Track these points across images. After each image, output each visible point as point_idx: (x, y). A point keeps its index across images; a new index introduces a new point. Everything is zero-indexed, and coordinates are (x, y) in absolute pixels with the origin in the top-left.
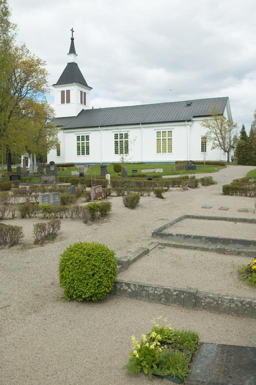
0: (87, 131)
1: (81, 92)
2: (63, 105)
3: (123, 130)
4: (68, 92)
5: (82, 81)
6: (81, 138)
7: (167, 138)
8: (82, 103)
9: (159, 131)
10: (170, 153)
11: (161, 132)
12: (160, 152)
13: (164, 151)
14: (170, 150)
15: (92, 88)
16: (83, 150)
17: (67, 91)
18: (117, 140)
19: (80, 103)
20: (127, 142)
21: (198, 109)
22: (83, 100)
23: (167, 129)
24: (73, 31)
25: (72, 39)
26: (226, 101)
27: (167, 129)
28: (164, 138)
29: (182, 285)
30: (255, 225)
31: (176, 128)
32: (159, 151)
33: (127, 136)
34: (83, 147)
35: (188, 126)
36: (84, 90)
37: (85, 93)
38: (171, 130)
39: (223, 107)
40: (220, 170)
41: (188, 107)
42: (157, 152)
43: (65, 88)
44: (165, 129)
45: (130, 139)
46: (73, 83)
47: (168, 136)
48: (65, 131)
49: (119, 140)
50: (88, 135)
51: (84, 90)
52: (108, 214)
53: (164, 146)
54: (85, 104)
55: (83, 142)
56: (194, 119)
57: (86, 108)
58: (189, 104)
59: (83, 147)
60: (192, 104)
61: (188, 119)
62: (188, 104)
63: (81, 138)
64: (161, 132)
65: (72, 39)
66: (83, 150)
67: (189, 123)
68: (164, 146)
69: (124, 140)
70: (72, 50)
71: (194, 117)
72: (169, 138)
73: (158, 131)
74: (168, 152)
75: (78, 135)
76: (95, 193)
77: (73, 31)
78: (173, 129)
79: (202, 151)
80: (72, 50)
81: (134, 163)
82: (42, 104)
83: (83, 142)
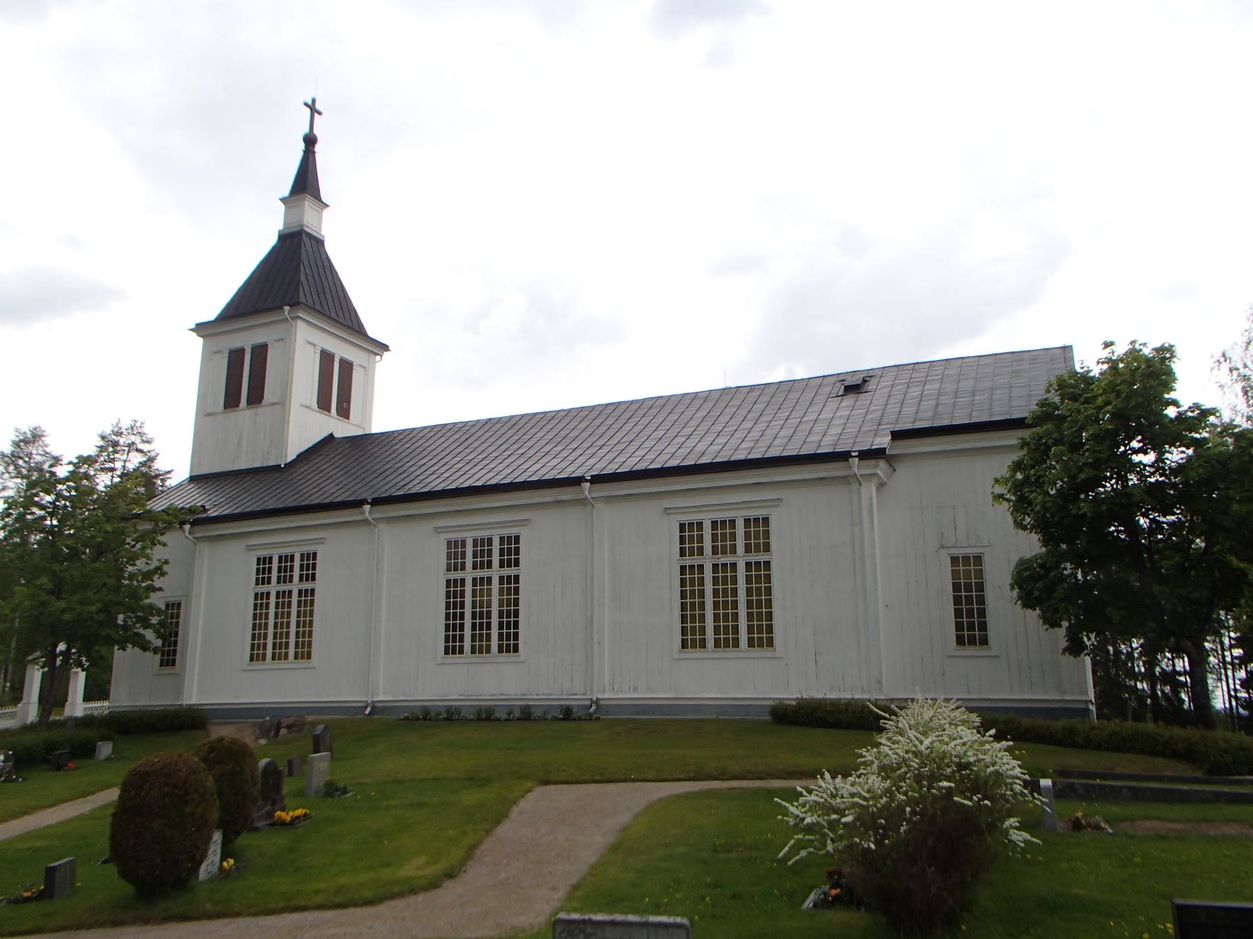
1: (326, 358)
2: (233, 415)
4: (260, 352)
8: (324, 404)
9: (695, 517)
10: (766, 652)
11: (740, 525)
12: (703, 644)
13: (727, 640)
14: (763, 637)
15: (385, 348)
16: (481, 626)
17: (254, 348)
18: (458, 575)
19: (315, 406)
20: (761, 574)
24: (313, 108)
25: (310, 141)
32: (691, 639)
33: (511, 551)
34: (724, 573)
36: (341, 350)
37: (347, 367)
38: (760, 513)
41: (849, 400)
42: (684, 645)
43: (246, 339)
47: (748, 549)
48: (201, 532)
50: (512, 531)
51: (341, 350)
52: (1041, 618)
53: (726, 604)
55: (479, 573)
57: (342, 429)
58: (855, 386)
59: (724, 573)
60: (871, 386)
65: (310, 141)
66: (481, 626)
67: (881, 467)
68: (726, 604)
72: (753, 558)
73: (687, 518)
74: (751, 643)
75: (264, 553)
77: (313, 108)
78: (321, 541)
81: (526, 715)
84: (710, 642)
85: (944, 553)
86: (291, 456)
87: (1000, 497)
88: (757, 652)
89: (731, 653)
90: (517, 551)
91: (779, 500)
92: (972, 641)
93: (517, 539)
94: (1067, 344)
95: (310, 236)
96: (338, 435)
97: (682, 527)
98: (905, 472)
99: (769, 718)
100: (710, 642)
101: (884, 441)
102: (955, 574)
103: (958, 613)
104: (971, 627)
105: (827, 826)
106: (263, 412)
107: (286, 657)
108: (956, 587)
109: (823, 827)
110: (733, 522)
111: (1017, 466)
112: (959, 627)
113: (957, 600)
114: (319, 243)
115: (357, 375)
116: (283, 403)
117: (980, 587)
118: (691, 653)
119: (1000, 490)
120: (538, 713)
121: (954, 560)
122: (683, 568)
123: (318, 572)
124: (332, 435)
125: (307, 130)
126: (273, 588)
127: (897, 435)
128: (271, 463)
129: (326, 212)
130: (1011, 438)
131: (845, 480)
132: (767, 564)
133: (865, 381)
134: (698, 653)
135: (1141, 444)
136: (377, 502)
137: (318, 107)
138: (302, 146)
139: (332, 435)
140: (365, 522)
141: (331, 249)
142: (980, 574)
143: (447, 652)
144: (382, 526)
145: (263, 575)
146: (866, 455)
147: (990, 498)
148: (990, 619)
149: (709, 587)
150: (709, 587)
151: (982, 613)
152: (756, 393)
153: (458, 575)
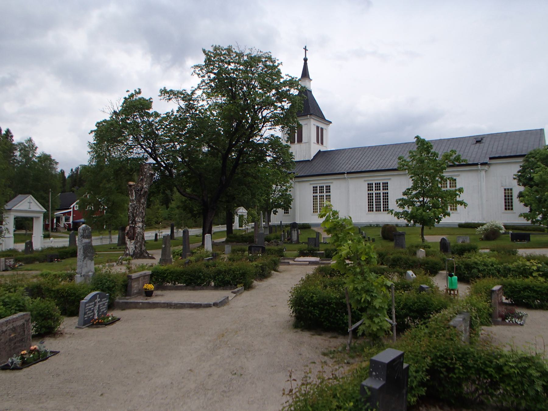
0: (371, 176)
1: (318, 127)
3: (380, 179)
5: (318, 114)
6: (318, 189)
12: (380, 210)
13: (378, 210)
15: (331, 122)
19: (316, 142)
22: (320, 139)
24: (305, 49)
25: (305, 60)
27: (382, 180)
29: (206, 303)
32: (370, 209)
34: (378, 195)
35: (483, 173)
36: (321, 125)
37: (322, 129)
41: (478, 144)
44: (323, 183)
45: (333, 193)
46: (307, 115)
51: (321, 125)
54: (322, 143)
55: (377, 192)
57: (323, 149)
58: (479, 140)
60: (483, 141)
61: (482, 162)
62: (477, 140)
63: (318, 189)
65: (305, 60)
67: (486, 167)
69: (374, 192)
71: (491, 158)
74: (384, 210)
77: (305, 49)
79: (506, 209)
83: (377, 192)
84: (374, 209)
85: (502, 187)
86: (312, 158)
87: (514, 179)
90: (387, 186)
91: (459, 175)
92: (509, 209)
93: (387, 183)
94: (543, 128)
95: (309, 91)
96: (321, 150)
98: (492, 168)
99: (458, 226)
100: (374, 209)
101: (487, 160)
102: (505, 193)
103: (505, 202)
104: (509, 206)
106: (302, 145)
108: (505, 196)
111: (519, 172)
112: (506, 206)
113: (505, 199)
114: (311, 92)
115: (324, 131)
116: (309, 142)
117: (512, 196)
118: (508, 211)
119: (515, 177)
120: (400, 225)
121: (505, 190)
123: (331, 190)
125: (304, 57)
127: (491, 158)
128: (307, 159)
129: (311, 82)
130: (521, 160)
131: (477, 170)
136: (348, 173)
138: (303, 62)
140: (345, 178)
141: (315, 94)
142: (511, 193)
143: (369, 211)
144: (349, 179)
145: (315, 191)
146: (483, 164)
147: (512, 179)
148: (514, 204)
151: (512, 202)
152: (449, 142)
153: (371, 192)
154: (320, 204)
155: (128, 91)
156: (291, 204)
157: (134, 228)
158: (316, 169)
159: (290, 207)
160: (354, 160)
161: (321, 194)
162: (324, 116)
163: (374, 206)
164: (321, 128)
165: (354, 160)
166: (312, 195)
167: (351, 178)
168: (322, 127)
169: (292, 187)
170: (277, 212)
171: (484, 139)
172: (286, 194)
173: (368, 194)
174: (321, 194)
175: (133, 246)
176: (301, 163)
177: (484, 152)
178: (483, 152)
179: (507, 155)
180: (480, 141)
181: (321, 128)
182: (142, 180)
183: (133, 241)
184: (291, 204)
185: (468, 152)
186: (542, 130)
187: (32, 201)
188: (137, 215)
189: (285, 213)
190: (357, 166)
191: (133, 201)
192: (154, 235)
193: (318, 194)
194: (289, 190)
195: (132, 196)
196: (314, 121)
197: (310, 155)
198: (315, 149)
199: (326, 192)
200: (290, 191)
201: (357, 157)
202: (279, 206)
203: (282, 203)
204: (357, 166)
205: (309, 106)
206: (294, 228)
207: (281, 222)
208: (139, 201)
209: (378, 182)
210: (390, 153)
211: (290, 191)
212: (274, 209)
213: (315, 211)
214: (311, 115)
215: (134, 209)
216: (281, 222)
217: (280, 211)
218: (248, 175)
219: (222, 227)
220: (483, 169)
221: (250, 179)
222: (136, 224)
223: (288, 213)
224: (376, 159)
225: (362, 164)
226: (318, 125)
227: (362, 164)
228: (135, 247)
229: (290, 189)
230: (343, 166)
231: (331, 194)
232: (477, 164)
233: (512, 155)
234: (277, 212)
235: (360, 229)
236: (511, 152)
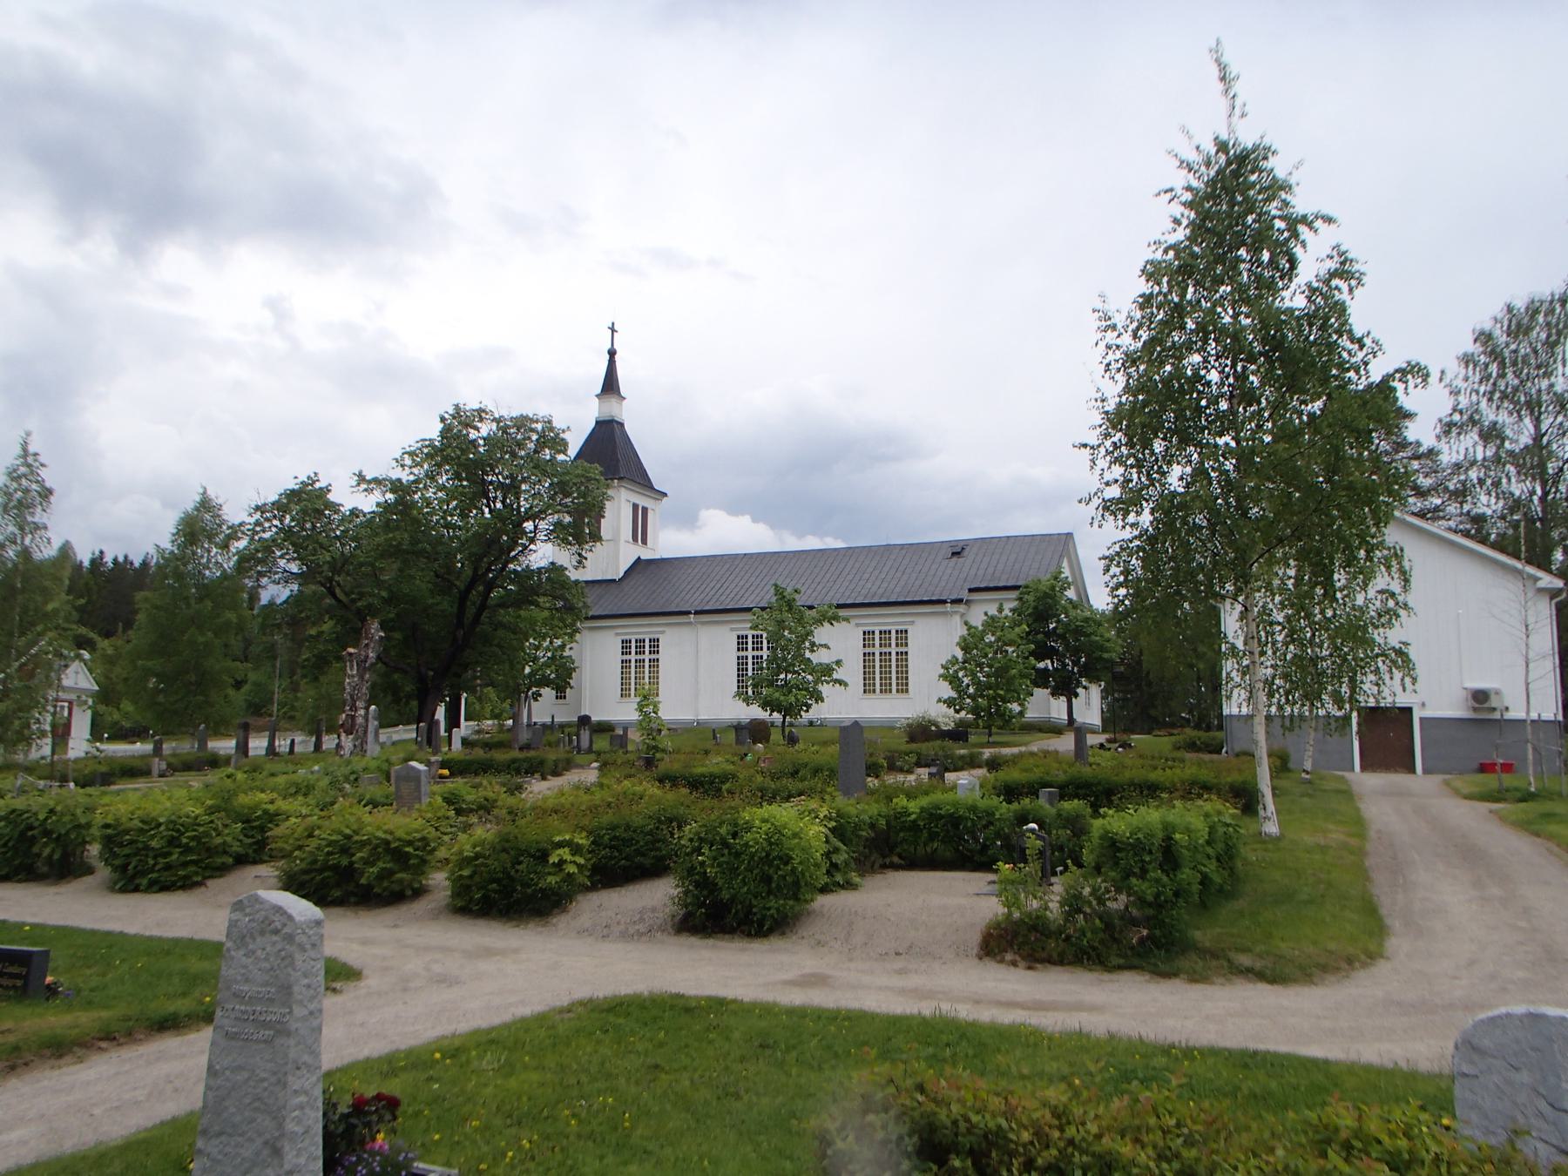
1: (635, 507)
5: (639, 478)
7: (877, 651)
11: (877, 633)
12: (874, 691)
13: (886, 690)
14: (903, 688)
15: (665, 495)
19: (631, 540)
21: (984, 566)
22: (640, 533)
23: (874, 624)
24: (613, 330)
25: (612, 353)
26: (1066, 544)
27: (874, 624)
28: (884, 650)
30: (321, 1175)
31: (668, 630)
34: (885, 656)
36: (642, 502)
37: (645, 510)
39: (1056, 557)
40: (210, 883)
41: (955, 559)
45: (664, 655)
47: (897, 645)
49: (750, 653)
51: (642, 502)
53: (886, 673)
54: (644, 542)
56: (842, 613)
57: (646, 554)
58: (957, 551)
59: (885, 656)
60: (965, 553)
61: (953, 598)
64: (877, 633)
65: (612, 353)
67: (961, 608)
68: (886, 673)
70: (610, 386)
71: (971, 590)
73: (867, 629)
74: (898, 691)
76: (68, 833)
77: (613, 330)
78: (663, 632)
80: (610, 386)
82: (185, 537)
84: (878, 690)
86: (621, 575)
88: (900, 695)
89: (888, 696)
97: (864, 633)
100: (878, 690)
101: (965, 595)
105: (396, 868)
107: (630, 695)
109: (391, 873)
110: (890, 632)
114: (622, 425)
116: (615, 540)
118: (867, 696)
122: (865, 654)
123: (660, 649)
124: (639, 558)
125: (610, 346)
126: (633, 657)
127: (971, 590)
128: (609, 577)
129: (624, 402)
131: (945, 614)
132: (906, 653)
133: (963, 549)
134: (872, 696)
135: (1161, 311)
136: (697, 613)
137: (616, 328)
138: (608, 357)
139: (639, 558)
140: (690, 623)
141: (630, 429)
144: (699, 626)
145: (626, 649)
149: (877, 664)
150: (877, 664)
154: (636, 678)
155: (296, 478)
156: (571, 678)
157: (353, 718)
158: (629, 601)
159: (569, 683)
160: (712, 585)
161: (639, 657)
162: (649, 480)
163: (894, 663)
164: (643, 508)
165: (712, 585)
166: (620, 657)
167: (703, 623)
168: (646, 505)
169: (576, 642)
170: (540, 695)
171: (968, 549)
172: (562, 657)
173: (738, 658)
174: (639, 657)
175: (351, 745)
176: (597, 586)
177: (962, 576)
178: (982, 566)
179: (1001, 584)
180: (958, 553)
181: (643, 508)
182: (367, 645)
183: (351, 737)
184: (571, 678)
185: (1001, 554)
186: (1069, 535)
187: (80, 670)
188: (358, 698)
189: (557, 698)
190: (717, 596)
191: (353, 676)
192: (289, 742)
193: (633, 657)
194: (568, 647)
195: (351, 669)
196: (628, 492)
197: (618, 568)
198: (628, 554)
199: (650, 653)
200: (571, 649)
201: (717, 578)
202: (545, 682)
203: (553, 676)
204: (717, 596)
205: (618, 461)
206: (584, 725)
207: (553, 717)
208: (362, 677)
209: (641, 637)
210: (786, 572)
211: (571, 649)
212: (534, 689)
213: (625, 693)
214: (620, 479)
215: (354, 688)
216: (553, 717)
217: (548, 693)
218: (501, 625)
219: (405, 731)
220: (956, 612)
221: (501, 632)
222: (356, 710)
223: (565, 697)
224: (756, 584)
225: (728, 592)
226: (637, 502)
227: (728, 592)
228: (355, 746)
229: (572, 645)
230: (687, 597)
231: (660, 656)
232: (944, 602)
233: (1009, 584)
234: (540, 695)
235: (714, 731)
236: (1008, 580)
